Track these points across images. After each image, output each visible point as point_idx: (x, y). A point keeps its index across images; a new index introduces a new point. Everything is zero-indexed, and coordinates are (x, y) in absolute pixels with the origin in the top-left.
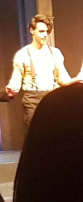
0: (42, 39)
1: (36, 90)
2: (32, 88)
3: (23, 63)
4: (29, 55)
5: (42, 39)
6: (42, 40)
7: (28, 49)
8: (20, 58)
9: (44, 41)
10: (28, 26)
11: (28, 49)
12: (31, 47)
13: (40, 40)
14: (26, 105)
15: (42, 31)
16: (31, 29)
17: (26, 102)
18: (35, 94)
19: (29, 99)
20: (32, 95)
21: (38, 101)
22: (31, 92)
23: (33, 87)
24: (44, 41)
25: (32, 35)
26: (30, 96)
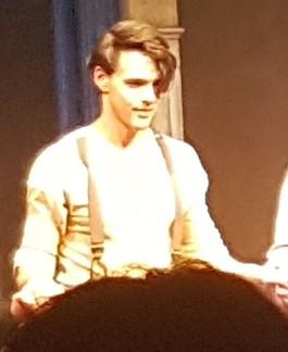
0: (135, 109)
3: (125, 144)
5: (135, 109)
7: (81, 143)
8: (54, 172)
11: (81, 143)
12: (95, 135)
16: (98, 71)
25: (99, 93)
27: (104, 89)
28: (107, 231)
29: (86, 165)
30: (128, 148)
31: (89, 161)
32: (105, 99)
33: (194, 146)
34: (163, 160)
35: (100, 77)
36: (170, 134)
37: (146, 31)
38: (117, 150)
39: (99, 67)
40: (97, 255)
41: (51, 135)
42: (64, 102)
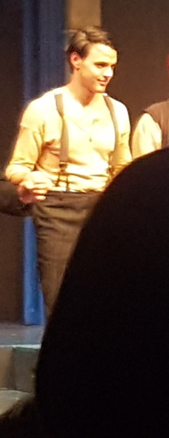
0: (99, 80)
1: (64, 189)
2: (57, 185)
3: (94, 149)
4: (61, 114)
5: (99, 80)
6: (98, 82)
7: (58, 98)
8: (41, 115)
9: (144, 130)
10: (66, 48)
11: (58, 98)
12: (67, 93)
13: (93, 83)
14: (41, 223)
15: (102, 65)
16: (73, 56)
17: (41, 214)
18: (61, 200)
19: (48, 210)
20: (55, 202)
21: (82, 215)
22: (55, 194)
23: (61, 184)
24: (144, 130)
25: (72, 68)
26: (53, 204)
27: (77, 67)
28: (72, 156)
29: (61, 114)
30: (87, 108)
31: (65, 112)
32: (75, 71)
33: (123, 103)
34: (108, 112)
35: (75, 59)
36: (75, 49)
37: (81, 38)
38: (79, 105)
39: (76, 53)
40: (63, 168)
41: (36, 93)
42: (28, 77)
